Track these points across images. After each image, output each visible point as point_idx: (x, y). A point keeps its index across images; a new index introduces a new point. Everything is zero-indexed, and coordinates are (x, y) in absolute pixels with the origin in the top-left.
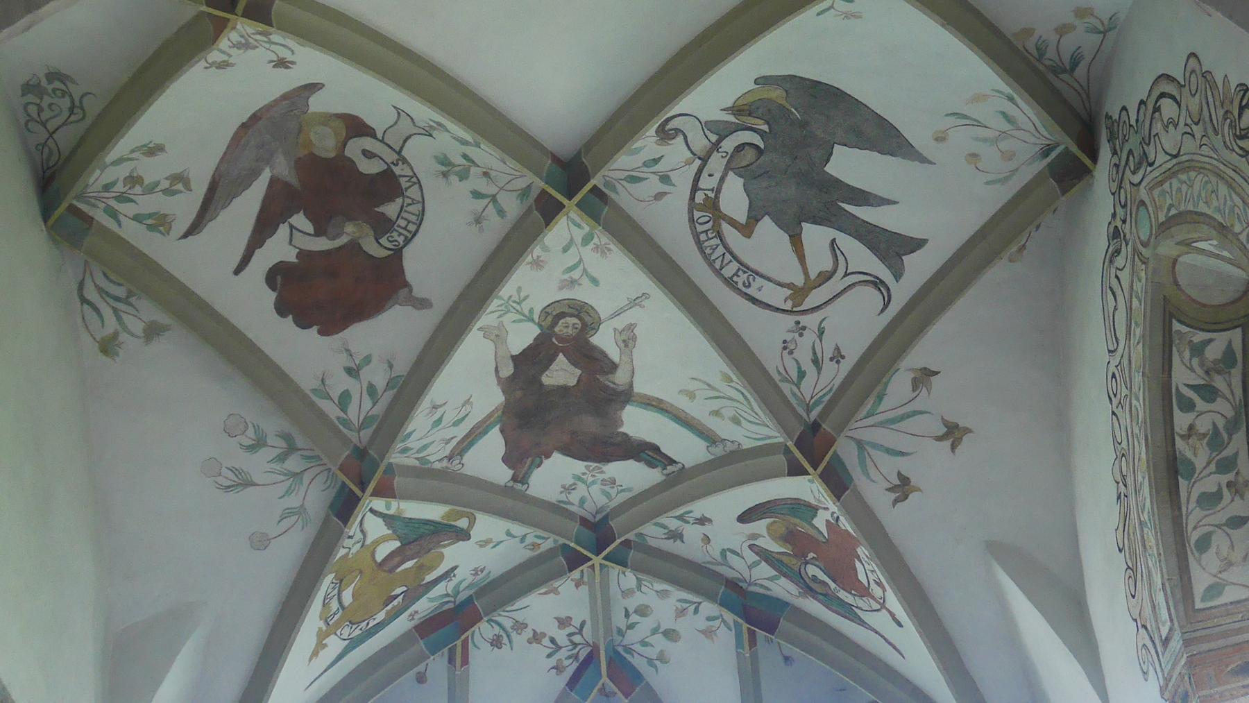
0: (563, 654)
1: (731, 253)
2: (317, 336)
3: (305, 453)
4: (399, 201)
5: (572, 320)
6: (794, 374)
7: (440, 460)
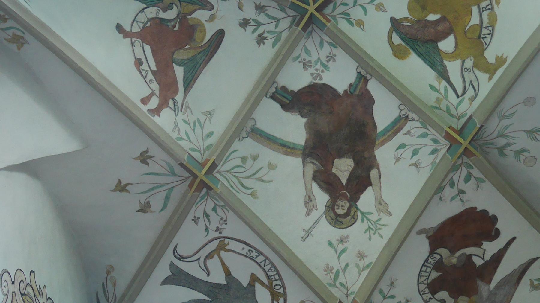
1: (261, 266)
2: (477, 207)
3: (494, 147)
4: (430, 281)
5: (340, 212)
6: (219, 210)
7: (413, 120)
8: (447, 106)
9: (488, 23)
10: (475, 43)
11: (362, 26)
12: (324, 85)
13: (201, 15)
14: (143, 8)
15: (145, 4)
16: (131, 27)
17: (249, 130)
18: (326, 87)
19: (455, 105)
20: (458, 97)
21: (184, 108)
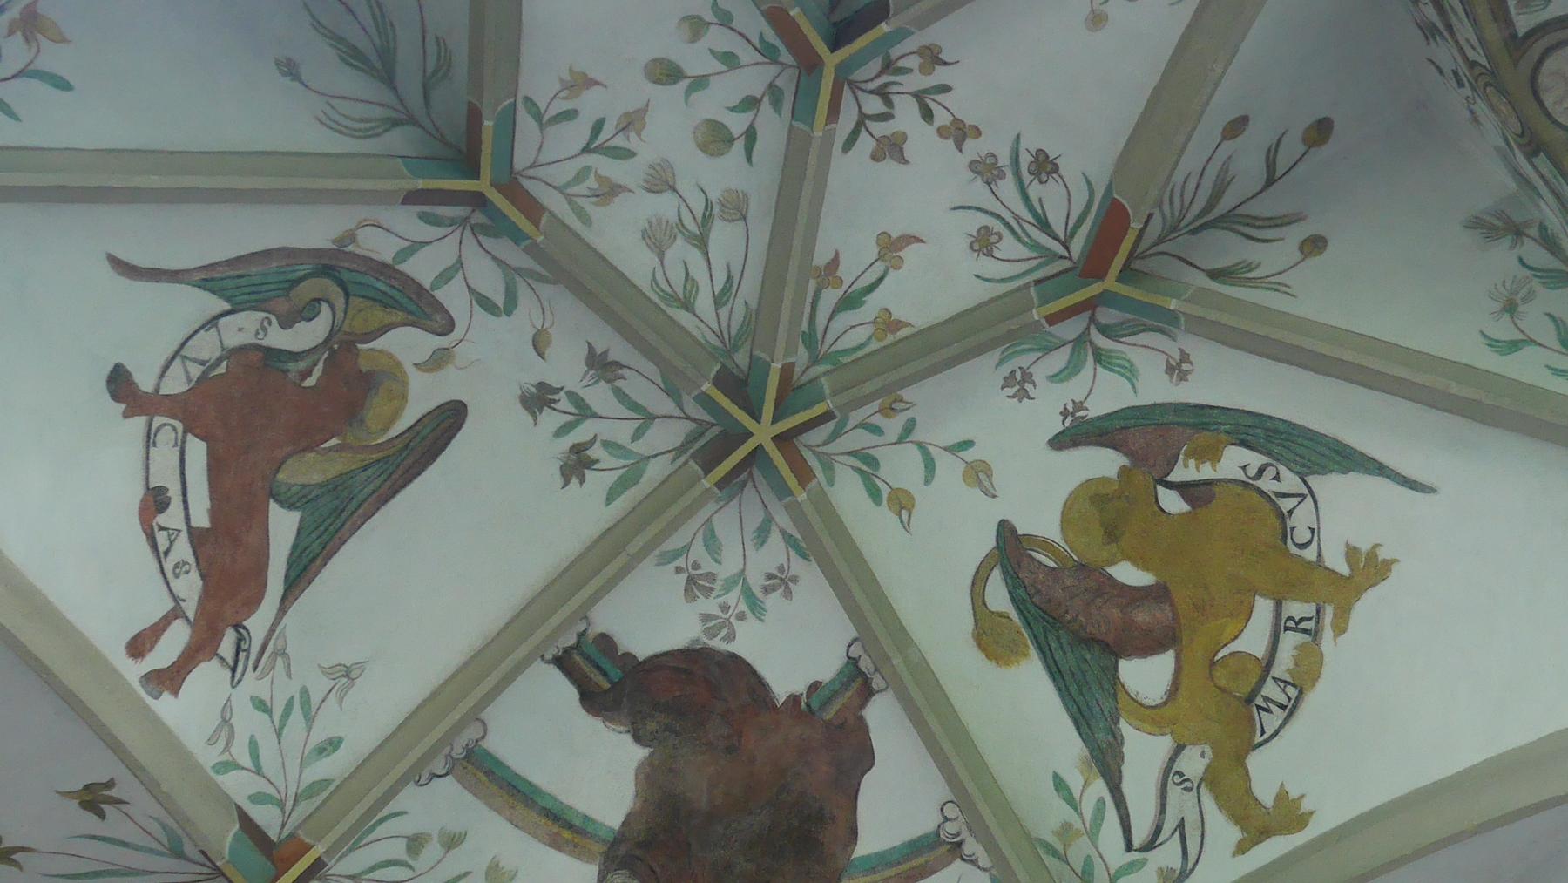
0: (917, 81)
7: (974, 862)
8: (1088, 862)
9: (1288, 671)
10: (1237, 712)
11: (905, 514)
12: (734, 658)
13: (405, 344)
14: (217, 311)
15: (228, 300)
16: (162, 376)
17: (458, 752)
18: (736, 665)
19: (1113, 867)
20: (1129, 847)
21: (266, 655)
